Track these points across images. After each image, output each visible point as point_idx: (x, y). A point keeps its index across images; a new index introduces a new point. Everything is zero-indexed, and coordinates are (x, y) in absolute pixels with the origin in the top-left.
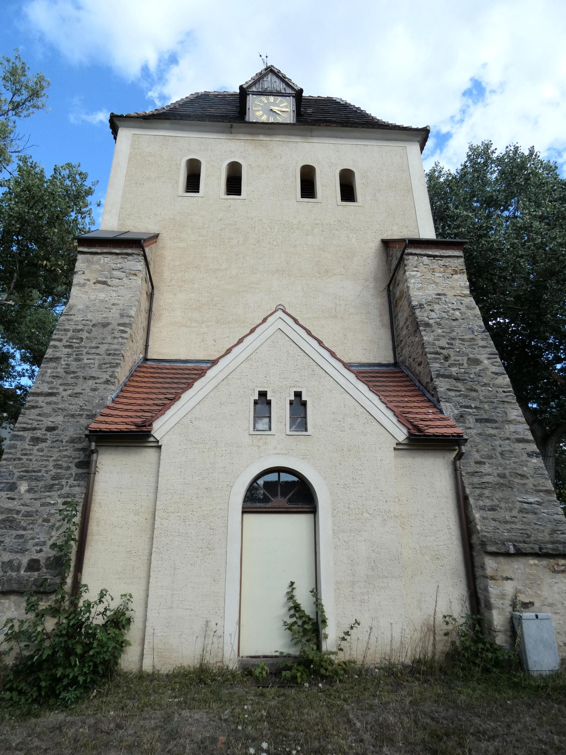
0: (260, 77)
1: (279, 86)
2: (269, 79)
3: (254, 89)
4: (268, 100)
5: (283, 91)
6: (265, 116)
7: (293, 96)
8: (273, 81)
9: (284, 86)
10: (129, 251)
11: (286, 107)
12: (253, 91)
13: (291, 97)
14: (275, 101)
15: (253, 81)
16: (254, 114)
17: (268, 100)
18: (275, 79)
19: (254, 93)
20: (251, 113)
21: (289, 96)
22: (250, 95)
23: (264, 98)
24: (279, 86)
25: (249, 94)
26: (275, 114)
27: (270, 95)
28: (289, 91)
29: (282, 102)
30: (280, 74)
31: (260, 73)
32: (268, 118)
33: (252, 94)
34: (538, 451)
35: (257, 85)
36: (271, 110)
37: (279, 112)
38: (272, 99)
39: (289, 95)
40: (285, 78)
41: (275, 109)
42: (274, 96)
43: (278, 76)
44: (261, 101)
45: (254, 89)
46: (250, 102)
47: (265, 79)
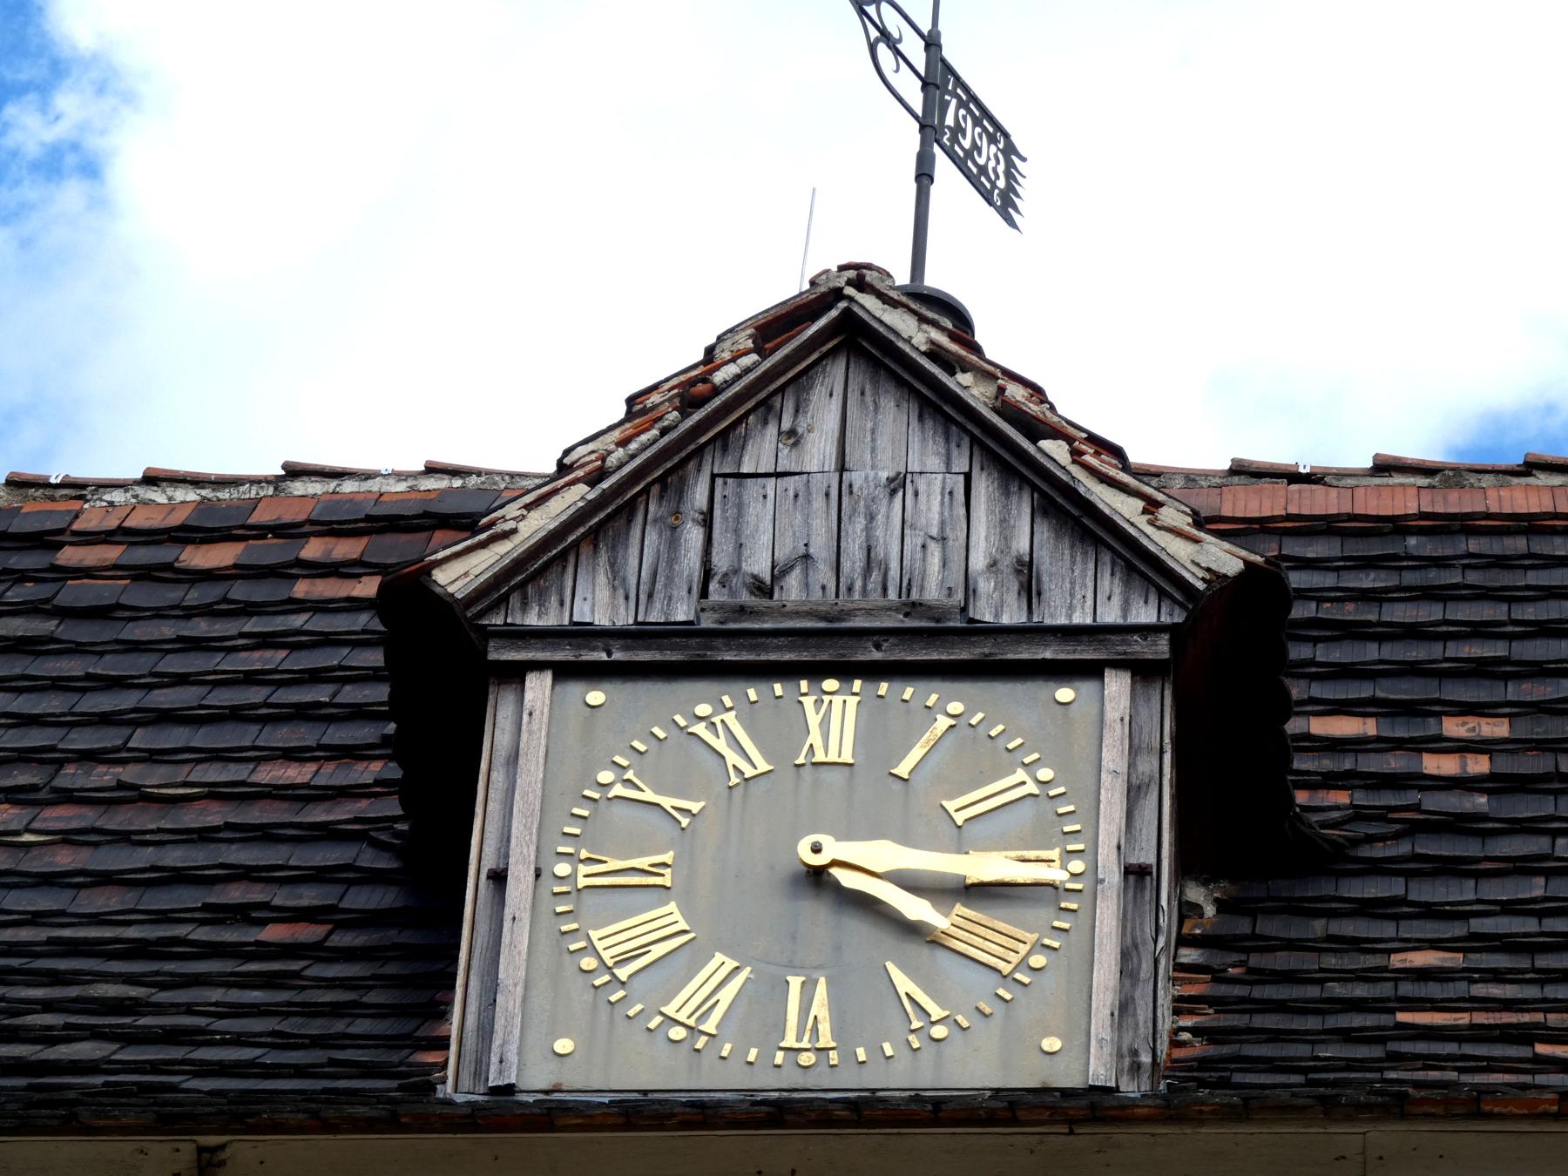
0: (692, 430)
1: (958, 539)
2: (819, 452)
3: (594, 600)
4: (781, 736)
5: (999, 606)
6: (1296, 765)
7: (1143, 672)
8: (867, 475)
9: (1025, 531)
10: (1126, 526)
11: (1038, 823)
12: (583, 634)
13: (1117, 685)
14: (879, 740)
15: (576, 496)
16: (561, 945)
17: (781, 736)
18: (894, 438)
19: (586, 658)
20: (517, 938)
21: (1091, 671)
22: (538, 687)
23: (723, 724)
24: (958, 539)
25: (515, 674)
26: (858, 929)
27: (816, 671)
28: (1085, 596)
29: (975, 758)
30: (967, 386)
31: (691, 390)
32: (760, 1010)
33: (564, 672)
34: (382, 628)
35: (643, 546)
36: (818, 878)
37: (915, 908)
38: (834, 717)
39: (1078, 656)
40: (1037, 429)
41: (871, 860)
42: (873, 671)
43: (940, 409)
44: (686, 761)
45: (594, 600)
46: (531, 772)
47: (761, 451)
